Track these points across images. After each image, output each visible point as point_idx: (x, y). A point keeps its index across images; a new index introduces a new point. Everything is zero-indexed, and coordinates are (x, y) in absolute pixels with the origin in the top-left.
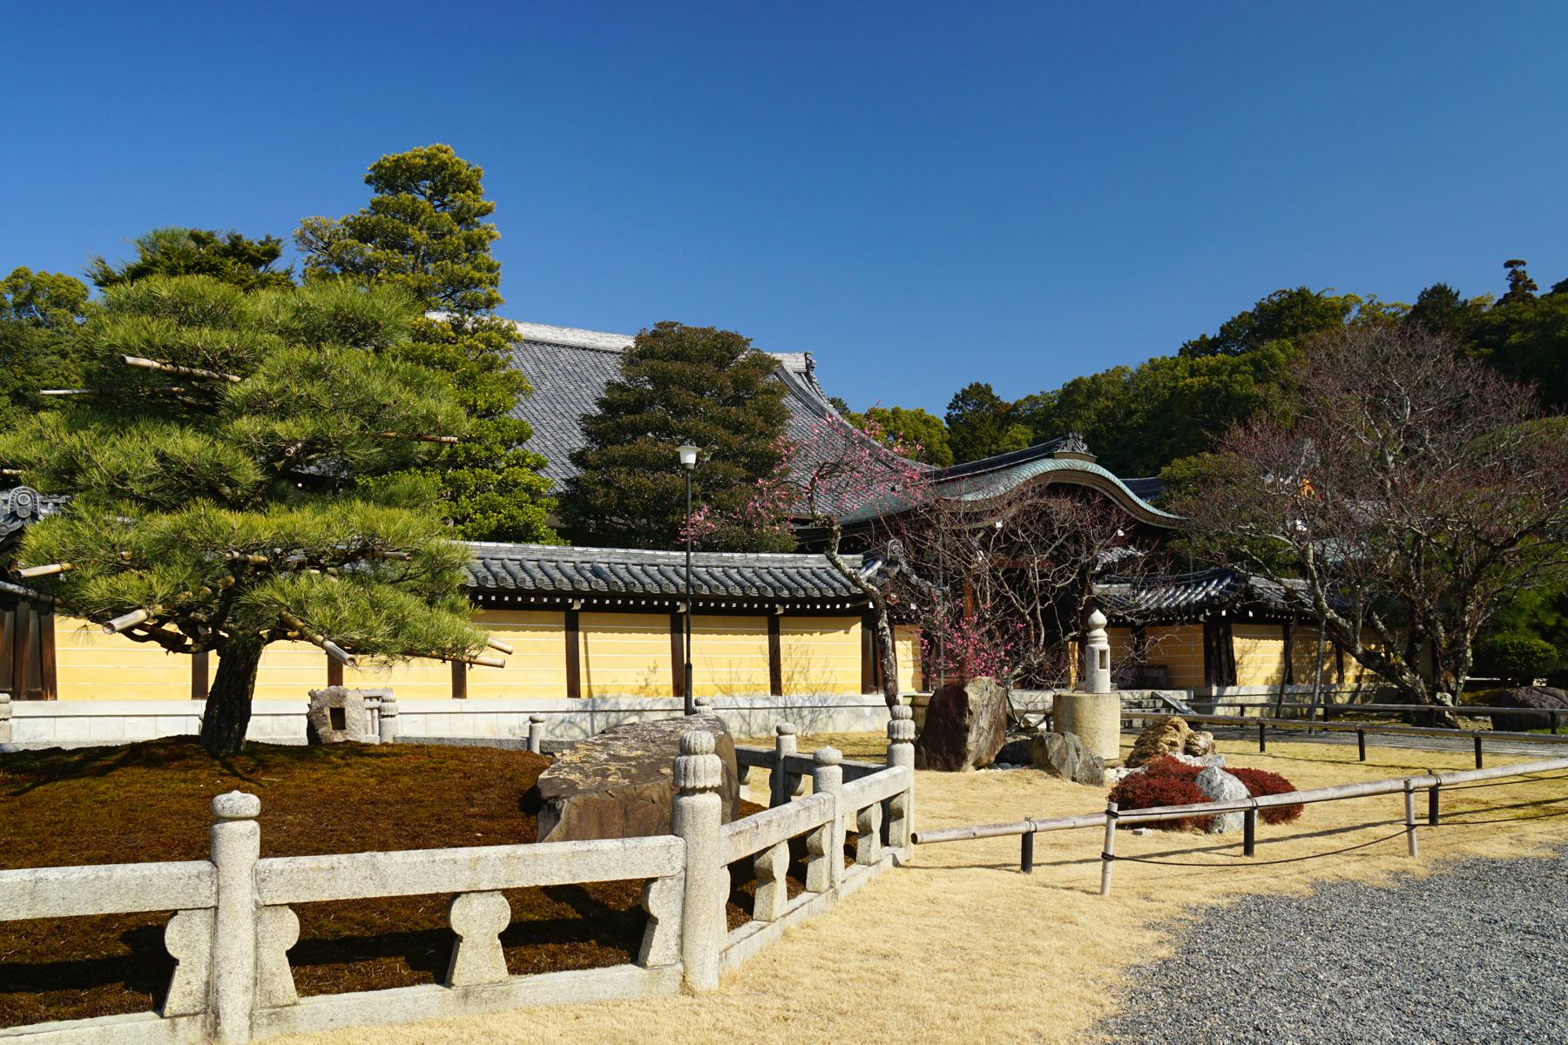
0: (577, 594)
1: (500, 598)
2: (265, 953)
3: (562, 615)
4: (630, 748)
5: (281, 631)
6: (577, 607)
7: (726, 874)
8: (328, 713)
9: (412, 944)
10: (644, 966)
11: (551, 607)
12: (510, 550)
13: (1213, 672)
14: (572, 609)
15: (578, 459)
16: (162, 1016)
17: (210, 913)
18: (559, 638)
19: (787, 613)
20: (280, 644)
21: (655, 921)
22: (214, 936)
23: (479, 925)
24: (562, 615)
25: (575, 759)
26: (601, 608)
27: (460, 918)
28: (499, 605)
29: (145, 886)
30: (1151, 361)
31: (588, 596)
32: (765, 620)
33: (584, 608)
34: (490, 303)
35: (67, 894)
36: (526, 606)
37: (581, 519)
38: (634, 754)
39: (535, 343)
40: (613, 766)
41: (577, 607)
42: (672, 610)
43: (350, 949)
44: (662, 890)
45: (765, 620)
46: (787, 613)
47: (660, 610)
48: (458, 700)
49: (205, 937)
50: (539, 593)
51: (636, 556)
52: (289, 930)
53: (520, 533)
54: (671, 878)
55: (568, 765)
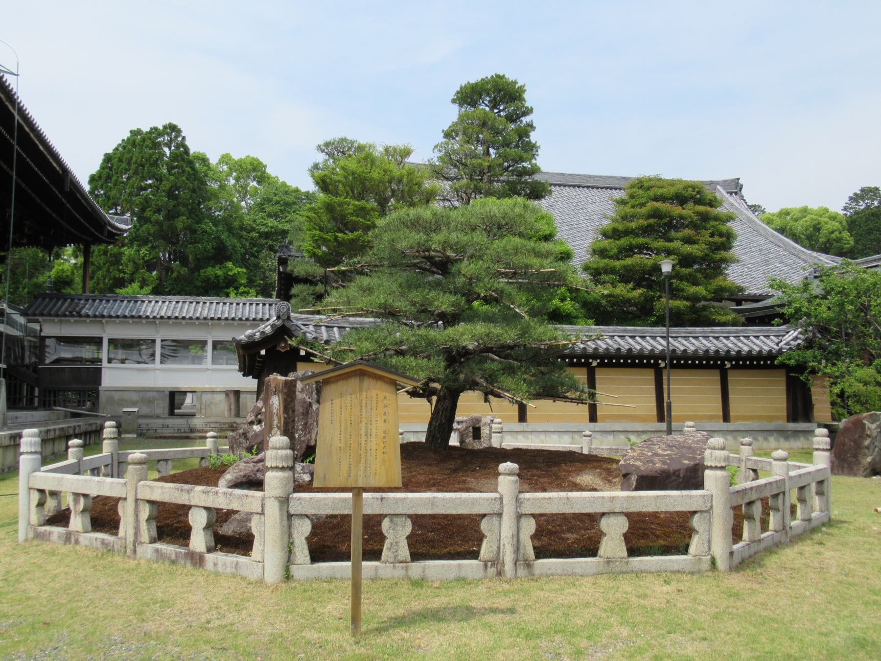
2: (522, 536)
4: (663, 450)
13: (262, 396)
17: (260, 511)
19: (733, 367)
22: (500, 526)
25: (635, 454)
26: (610, 365)
29: (432, 502)
30: (131, 132)
32: (585, 370)
33: (599, 365)
38: (666, 453)
40: (656, 459)
41: (595, 364)
42: (656, 366)
45: (717, 372)
46: (733, 367)
48: (725, 424)
49: (497, 527)
52: (529, 527)
55: (633, 457)
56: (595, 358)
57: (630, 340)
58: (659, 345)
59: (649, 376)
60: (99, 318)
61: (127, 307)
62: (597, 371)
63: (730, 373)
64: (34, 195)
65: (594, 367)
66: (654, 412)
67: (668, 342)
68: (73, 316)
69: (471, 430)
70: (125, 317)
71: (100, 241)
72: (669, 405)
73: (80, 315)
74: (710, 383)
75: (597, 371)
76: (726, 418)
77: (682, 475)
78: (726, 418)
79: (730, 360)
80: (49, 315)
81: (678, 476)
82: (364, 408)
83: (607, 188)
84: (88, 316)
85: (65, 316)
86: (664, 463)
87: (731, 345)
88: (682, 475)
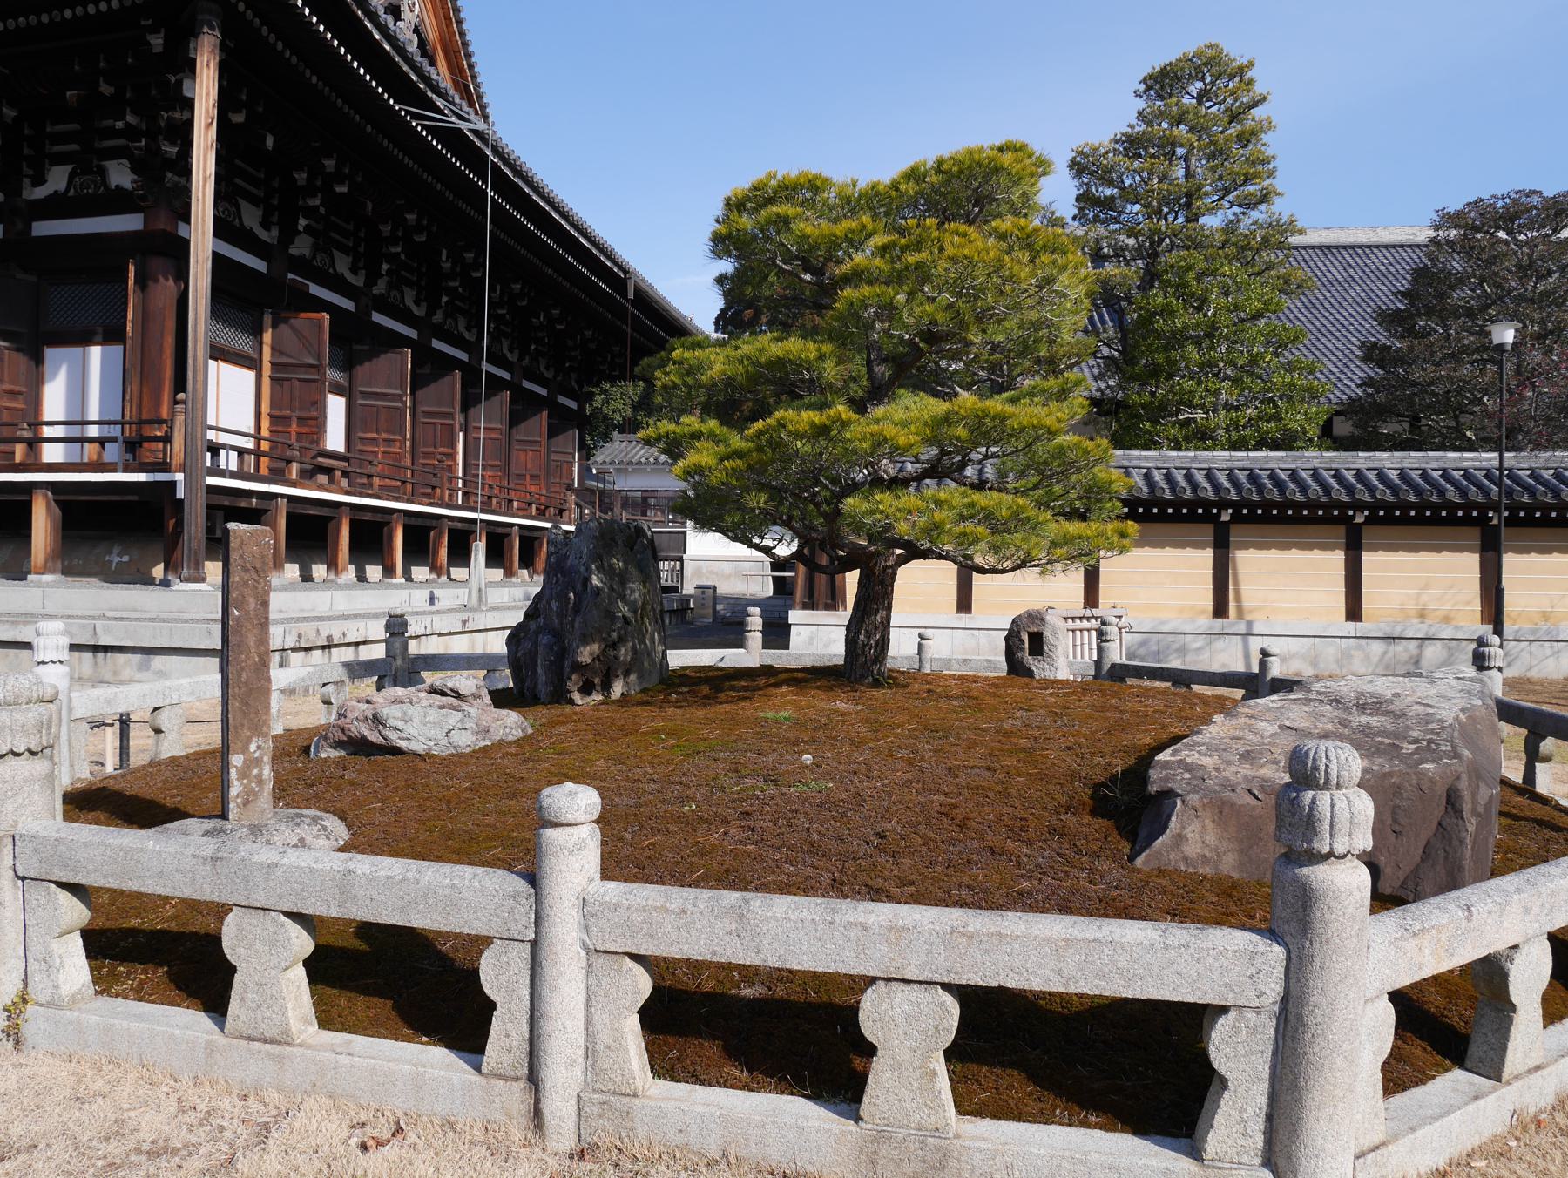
0: (1359, 506)
1: (1177, 511)
3: (1342, 529)
5: (914, 552)
6: (1359, 519)
7: (1386, 1014)
8: (1025, 638)
9: (800, 1039)
10: (1196, 1153)
11: (1328, 520)
12: (1281, 459)
14: (1353, 523)
15: (1372, 353)
16: (478, 1069)
18: (1338, 558)
20: (916, 565)
21: (1224, 1083)
23: (909, 1035)
24: (1342, 529)
26: (1389, 521)
27: (878, 1015)
28: (1162, 518)
31: (1373, 507)
33: (1368, 521)
34: (1265, 197)
35: (374, 894)
36: (1298, 520)
37: (1358, 425)
39: (1345, 248)
41: (1359, 519)
42: (1482, 521)
43: (715, 1024)
44: (1236, 1030)
47: (1467, 521)
50: (1313, 505)
51: (1437, 459)
52: (642, 984)
53: (1286, 442)
54: (1257, 1010)
62: (1234, 529)
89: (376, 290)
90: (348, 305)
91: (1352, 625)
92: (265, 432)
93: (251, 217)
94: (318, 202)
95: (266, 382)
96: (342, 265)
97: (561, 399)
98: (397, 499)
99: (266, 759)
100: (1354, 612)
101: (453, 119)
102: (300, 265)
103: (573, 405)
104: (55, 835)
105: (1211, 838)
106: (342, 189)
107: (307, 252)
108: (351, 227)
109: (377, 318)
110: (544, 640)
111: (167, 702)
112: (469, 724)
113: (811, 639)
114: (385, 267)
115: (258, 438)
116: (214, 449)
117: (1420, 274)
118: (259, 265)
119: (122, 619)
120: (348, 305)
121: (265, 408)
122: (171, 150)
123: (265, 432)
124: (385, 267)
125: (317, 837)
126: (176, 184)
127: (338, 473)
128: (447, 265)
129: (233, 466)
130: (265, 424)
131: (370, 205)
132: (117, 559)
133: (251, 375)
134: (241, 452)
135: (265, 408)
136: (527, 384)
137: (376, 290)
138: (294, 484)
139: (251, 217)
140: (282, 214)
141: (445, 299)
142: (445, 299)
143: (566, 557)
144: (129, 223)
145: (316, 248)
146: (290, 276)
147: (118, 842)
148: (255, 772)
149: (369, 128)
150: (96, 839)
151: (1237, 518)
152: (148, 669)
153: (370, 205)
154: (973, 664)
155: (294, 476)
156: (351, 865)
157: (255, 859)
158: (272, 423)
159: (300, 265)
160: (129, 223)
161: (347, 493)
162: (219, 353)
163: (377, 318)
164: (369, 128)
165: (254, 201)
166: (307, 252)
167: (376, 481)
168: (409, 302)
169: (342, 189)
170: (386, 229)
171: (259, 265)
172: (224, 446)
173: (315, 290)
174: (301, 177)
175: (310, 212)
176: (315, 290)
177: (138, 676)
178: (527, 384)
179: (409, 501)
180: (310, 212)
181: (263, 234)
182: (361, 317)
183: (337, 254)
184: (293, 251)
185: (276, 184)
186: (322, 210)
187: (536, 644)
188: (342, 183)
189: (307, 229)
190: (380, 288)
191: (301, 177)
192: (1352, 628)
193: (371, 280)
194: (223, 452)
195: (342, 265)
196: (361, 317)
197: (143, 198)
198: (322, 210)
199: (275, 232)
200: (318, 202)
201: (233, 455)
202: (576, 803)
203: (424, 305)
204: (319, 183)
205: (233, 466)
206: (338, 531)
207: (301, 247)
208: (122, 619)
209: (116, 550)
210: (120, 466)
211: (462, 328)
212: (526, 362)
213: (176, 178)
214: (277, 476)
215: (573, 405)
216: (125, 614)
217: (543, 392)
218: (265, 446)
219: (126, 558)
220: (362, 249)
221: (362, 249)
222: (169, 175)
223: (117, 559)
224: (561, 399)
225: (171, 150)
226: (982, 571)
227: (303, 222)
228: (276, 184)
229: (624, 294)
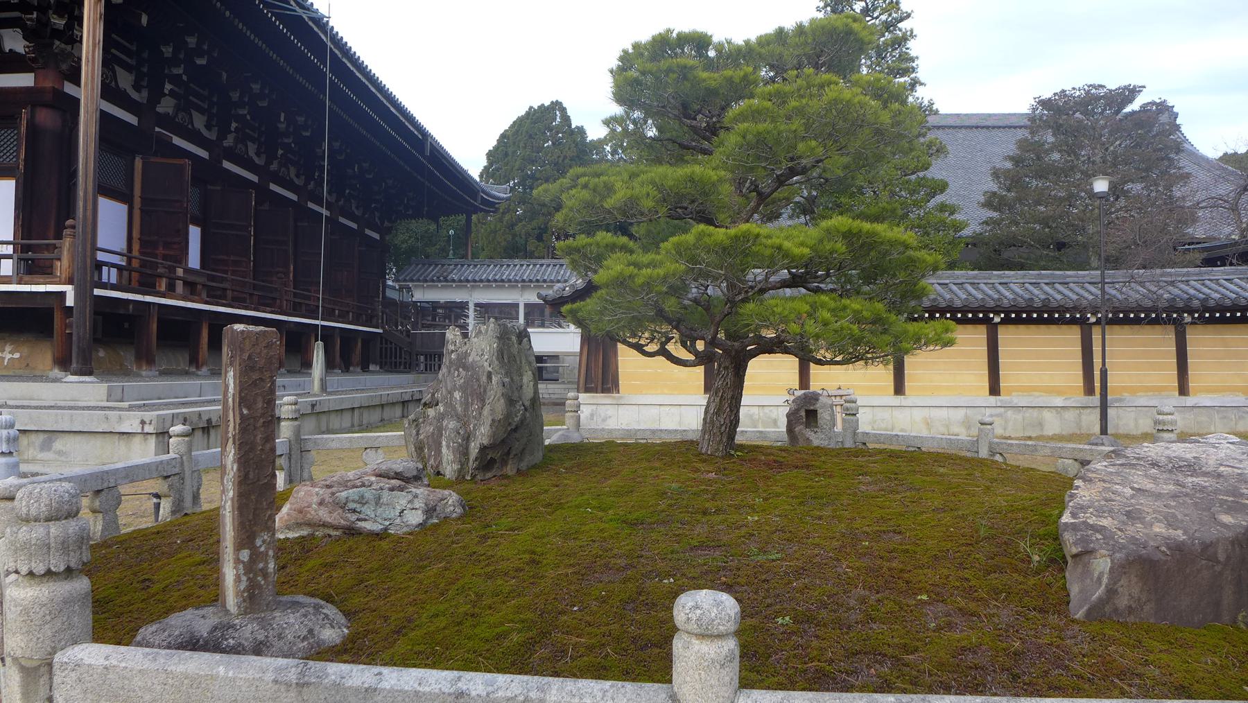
26: (1018, 321)
33: (1003, 322)
37: (993, 254)
41: (997, 320)
45: (1171, 328)
56: (997, 313)
57: (1046, 288)
58: (1090, 294)
59: (1073, 335)
60: (463, 283)
61: (499, 271)
62: (1001, 329)
63: (1189, 329)
64: (402, 163)
65: (997, 324)
66: (1080, 382)
67: (1103, 290)
68: (440, 281)
69: (803, 414)
70: (489, 281)
71: (476, 210)
72: (1104, 373)
73: (446, 281)
74: (1161, 341)
75: (1001, 329)
76: (1183, 390)
77: (1222, 557)
78: (1183, 390)
79: (1191, 313)
80: (418, 280)
81: (1214, 559)
82: (31, 479)
83: (1010, 127)
84: (453, 281)
85: (433, 281)
86: (1171, 522)
87: (1192, 292)
88: (1222, 557)
89: (226, 144)
90: (204, 154)
91: (993, 399)
92: (135, 253)
93: (125, 80)
94: (181, 72)
95: (137, 213)
96: (199, 122)
97: (368, 232)
98: (246, 308)
99: (271, 553)
100: (994, 390)
101: (297, 9)
102: (164, 121)
103: (376, 236)
104: (102, 661)
105: (1136, 591)
106: (201, 61)
107: (170, 111)
108: (206, 93)
109: (227, 165)
110: (452, 424)
111: (105, 485)
112: (419, 504)
113: (592, 415)
114: (234, 125)
115: (129, 260)
116: (99, 266)
117: (1023, 144)
118: (132, 119)
119: (23, 407)
120: (204, 154)
121: (136, 234)
122: (59, 22)
123: (135, 253)
124: (234, 125)
125: (323, 626)
126: (63, 51)
127: (199, 287)
128: (282, 126)
129: (114, 280)
130: (136, 247)
131: (225, 75)
132: (10, 356)
133: (125, 208)
134: (120, 268)
135: (136, 234)
136: (342, 220)
137: (226, 144)
138: (164, 296)
139: (125, 80)
140: (152, 80)
141: (280, 152)
142: (280, 152)
143: (466, 354)
144: (24, 80)
145: (178, 108)
146: (157, 129)
147: (181, 668)
148: (261, 565)
149: (228, 13)
150: (154, 666)
151: (1007, 321)
152: (49, 449)
153: (225, 75)
154: (747, 435)
155: (163, 288)
156: (462, 685)
157: (349, 683)
158: (141, 246)
159: (164, 121)
160: (24, 80)
161: (206, 303)
162: (104, 189)
163: (227, 165)
164: (228, 13)
165: (128, 68)
166: (170, 111)
167: (229, 293)
168: (252, 153)
169: (201, 61)
170: (235, 96)
171: (132, 119)
172: (106, 264)
173: (177, 141)
174: (167, 51)
175: (175, 80)
176: (177, 141)
177: (41, 456)
178: (342, 220)
179: (255, 309)
180: (175, 80)
181: (135, 95)
182: (214, 163)
183: (195, 114)
184: (159, 109)
185: (145, 55)
186: (185, 78)
187: (440, 430)
188: (201, 56)
189: (172, 93)
190: (229, 141)
191: (167, 51)
192: (993, 400)
193: (223, 135)
194: (105, 269)
195: (199, 122)
196: (214, 163)
197: (34, 60)
198: (185, 78)
199: (145, 93)
200: (181, 72)
201: (114, 271)
202: (706, 611)
203: (264, 156)
204: (182, 56)
205: (114, 280)
206: (199, 333)
207: (166, 106)
208: (23, 407)
209: (8, 348)
210: (15, 278)
211: (292, 175)
212: (341, 203)
213: (63, 46)
214: (147, 286)
215: (376, 236)
216: (25, 403)
217: (354, 226)
218: (135, 264)
219: (17, 355)
220: (214, 111)
221: (214, 111)
222: (57, 43)
223: (10, 356)
224: (368, 232)
225: (59, 22)
226: (819, 362)
227: (168, 87)
228: (145, 55)
229: (422, 152)
